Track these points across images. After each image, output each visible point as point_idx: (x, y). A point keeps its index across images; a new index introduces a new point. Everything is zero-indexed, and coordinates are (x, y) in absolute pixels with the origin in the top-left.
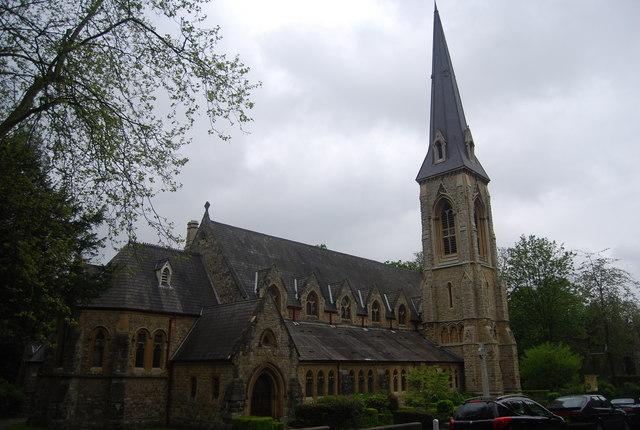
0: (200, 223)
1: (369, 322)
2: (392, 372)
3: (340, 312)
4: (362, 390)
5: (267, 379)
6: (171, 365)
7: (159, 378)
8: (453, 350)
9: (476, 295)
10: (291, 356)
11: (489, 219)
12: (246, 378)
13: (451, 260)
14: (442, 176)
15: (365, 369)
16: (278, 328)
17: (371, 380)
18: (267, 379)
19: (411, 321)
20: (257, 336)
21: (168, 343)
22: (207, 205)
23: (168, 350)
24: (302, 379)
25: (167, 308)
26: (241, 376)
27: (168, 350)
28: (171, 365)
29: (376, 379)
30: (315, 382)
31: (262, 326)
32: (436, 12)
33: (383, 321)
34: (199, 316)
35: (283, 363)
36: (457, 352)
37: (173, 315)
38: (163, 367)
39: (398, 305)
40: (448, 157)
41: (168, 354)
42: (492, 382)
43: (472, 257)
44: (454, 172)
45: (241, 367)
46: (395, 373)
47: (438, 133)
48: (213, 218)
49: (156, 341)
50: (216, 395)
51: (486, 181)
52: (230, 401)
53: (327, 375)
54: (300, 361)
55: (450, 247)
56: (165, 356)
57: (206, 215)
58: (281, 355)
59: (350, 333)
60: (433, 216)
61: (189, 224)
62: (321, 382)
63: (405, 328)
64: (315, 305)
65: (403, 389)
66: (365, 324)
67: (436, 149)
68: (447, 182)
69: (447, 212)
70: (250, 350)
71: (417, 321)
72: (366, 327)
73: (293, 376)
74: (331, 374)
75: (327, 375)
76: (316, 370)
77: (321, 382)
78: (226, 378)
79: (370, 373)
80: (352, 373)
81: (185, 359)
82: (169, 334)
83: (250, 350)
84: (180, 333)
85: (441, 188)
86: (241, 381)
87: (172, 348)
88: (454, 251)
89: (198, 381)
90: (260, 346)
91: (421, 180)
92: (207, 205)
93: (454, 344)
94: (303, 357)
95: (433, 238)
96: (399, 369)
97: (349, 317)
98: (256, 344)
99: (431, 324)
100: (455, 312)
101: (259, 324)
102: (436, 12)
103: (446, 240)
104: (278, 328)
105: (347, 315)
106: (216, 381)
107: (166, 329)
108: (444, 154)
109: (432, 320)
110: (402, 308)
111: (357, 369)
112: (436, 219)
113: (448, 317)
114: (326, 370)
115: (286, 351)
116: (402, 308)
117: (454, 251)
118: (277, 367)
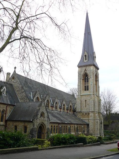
0: (11, 75)
1: (62, 111)
2: (71, 127)
3: (55, 107)
4: (54, 132)
5: (41, 127)
6: (6, 121)
7: (2, 125)
8: (85, 121)
9: (94, 104)
10: (48, 121)
11: (95, 146)
12: (36, 127)
13: (87, 93)
14: (86, 66)
15: (65, 125)
16: (45, 112)
17: (66, 129)
18: (41, 127)
19: (51, 106)
20: (40, 114)
21: (6, 114)
22: (15, 68)
23: (5, 116)
24: (50, 128)
25: (5, 102)
26: (35, 126)
27: (5, 116)
28: (6, 121)
29: (68, 128)
30: (53, 129)
31: (41, 111)
32: (87, 13)
33: (66, 111)
34: (15, 105)
35: (46, 123)
36: (87, 121)
37: (8, 105)
38: (4, 121)
39: (70, 106)
40: (88, 60)
41: (5, 118)
42: (72, 131)
43: (94, 92)
44: (90, 65)
45: (35, 124)
46: (54, 126)
47: (86, 52)
48: (17, 72)
49: (2, 113)
50: (25, 132)
51: (98, 69)
52: (32, 134)
53: (56, 127)
54: (50, 122)
55: (86, 88)
56: (4, 118)
57: (15, 71)
58: (45, 120)
59: (58, 113)
60: (82, 79)
61: (7, 73)
62: (54, 129)
63: (71, 113)
64: (48, 104)
65: (74, 132)
66: (61, 111)
67: (84, 57)
68: (88, 68)
69: (86, 77)
70: (38, 118)
71: (74, 111)
72: (61, 112)
73: (48, 127)
74: (57, 126)
75: (56, 127)
76: (53, 125)
77: (54, 129)
78: (30, 127)
79: (66, 127)
80: (62, 126)
81: (11, 119)
82: (6, 111)
83: (38, 118)
84: (9, 111)
85: (85, 70)
86: (35, 128)
87: (7, 116)
88: (88, 90)
89: (18, 127)
90: (40, 117)
91: (79, 66)
92: (15, 68)
93: (86, 119)
94: (52, 121)
95: (81, 85)
96: (73, 126)
97: (57, 109)
98: (39, 117)
99: (79, 112)
100: (87, 109)
101: (40, 110)
102: (87, 13)
103: (85, 86)
104: (45, 112)
105: (56, 108)
106: (26, 128)
107: (5, 109)
108: (87, 59)
109: (79, 111)
110: (71, 106)
111: (63, 125)
112: (83, 79)
113: (84, 110)
114: (56, 125)
115: (46, 119)
116: (71, 106)
117: (88, 90)
118: (44, 124)
